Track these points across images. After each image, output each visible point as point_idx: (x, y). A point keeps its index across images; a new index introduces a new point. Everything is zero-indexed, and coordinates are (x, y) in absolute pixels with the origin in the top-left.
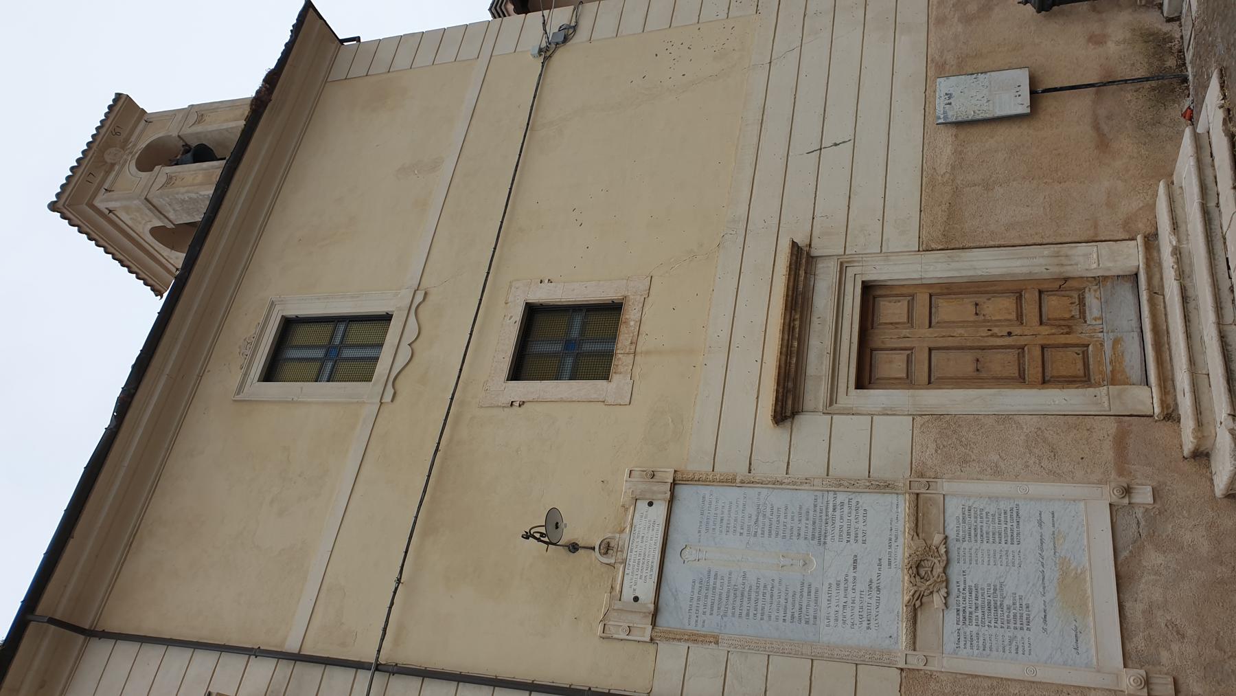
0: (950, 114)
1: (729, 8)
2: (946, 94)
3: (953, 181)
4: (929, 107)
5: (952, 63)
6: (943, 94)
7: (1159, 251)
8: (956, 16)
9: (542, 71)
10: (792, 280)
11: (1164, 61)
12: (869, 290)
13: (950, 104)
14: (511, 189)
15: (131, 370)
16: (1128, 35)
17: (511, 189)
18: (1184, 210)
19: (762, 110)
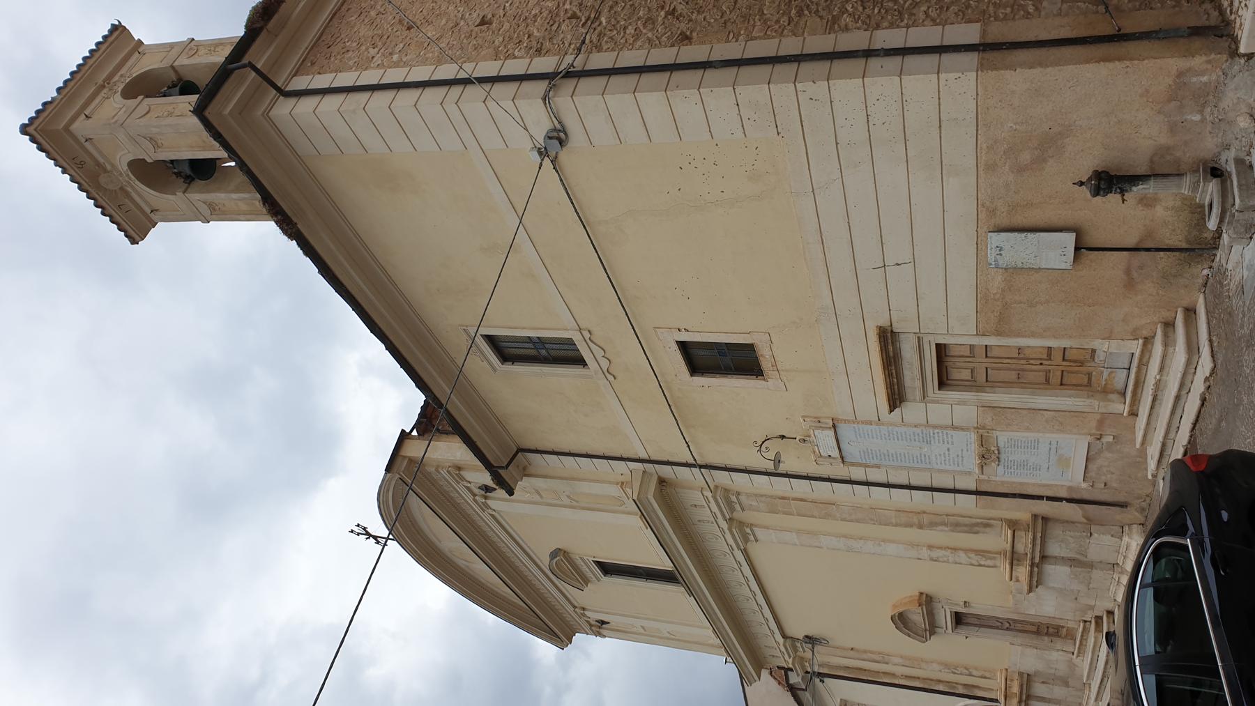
0: (1001, 262)
1: (743, 126)
2: (997, 247)
3: (1003, 299)
4: (981, 244)
5: (1003, 210)
6: (994, 246)
7: (1153, 345)
8: (1007, 164)
9: (560, 176)
10: (884, 354)
11: (1203, 232)
12: (941, 349)
13: (1001, 255)
14: (608, 276)
15: (308, 258)
16: (1179, 203)
17: (608, 276)
18: (1171, 360)
19: (819, 233)
